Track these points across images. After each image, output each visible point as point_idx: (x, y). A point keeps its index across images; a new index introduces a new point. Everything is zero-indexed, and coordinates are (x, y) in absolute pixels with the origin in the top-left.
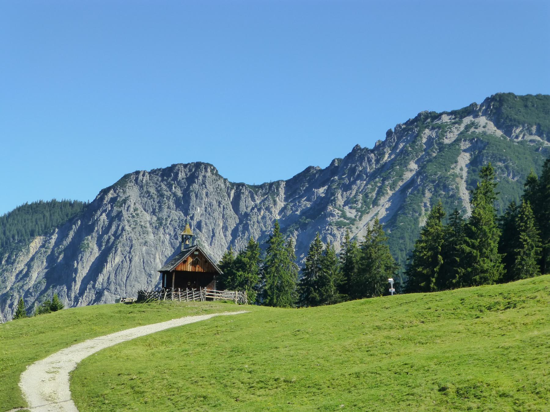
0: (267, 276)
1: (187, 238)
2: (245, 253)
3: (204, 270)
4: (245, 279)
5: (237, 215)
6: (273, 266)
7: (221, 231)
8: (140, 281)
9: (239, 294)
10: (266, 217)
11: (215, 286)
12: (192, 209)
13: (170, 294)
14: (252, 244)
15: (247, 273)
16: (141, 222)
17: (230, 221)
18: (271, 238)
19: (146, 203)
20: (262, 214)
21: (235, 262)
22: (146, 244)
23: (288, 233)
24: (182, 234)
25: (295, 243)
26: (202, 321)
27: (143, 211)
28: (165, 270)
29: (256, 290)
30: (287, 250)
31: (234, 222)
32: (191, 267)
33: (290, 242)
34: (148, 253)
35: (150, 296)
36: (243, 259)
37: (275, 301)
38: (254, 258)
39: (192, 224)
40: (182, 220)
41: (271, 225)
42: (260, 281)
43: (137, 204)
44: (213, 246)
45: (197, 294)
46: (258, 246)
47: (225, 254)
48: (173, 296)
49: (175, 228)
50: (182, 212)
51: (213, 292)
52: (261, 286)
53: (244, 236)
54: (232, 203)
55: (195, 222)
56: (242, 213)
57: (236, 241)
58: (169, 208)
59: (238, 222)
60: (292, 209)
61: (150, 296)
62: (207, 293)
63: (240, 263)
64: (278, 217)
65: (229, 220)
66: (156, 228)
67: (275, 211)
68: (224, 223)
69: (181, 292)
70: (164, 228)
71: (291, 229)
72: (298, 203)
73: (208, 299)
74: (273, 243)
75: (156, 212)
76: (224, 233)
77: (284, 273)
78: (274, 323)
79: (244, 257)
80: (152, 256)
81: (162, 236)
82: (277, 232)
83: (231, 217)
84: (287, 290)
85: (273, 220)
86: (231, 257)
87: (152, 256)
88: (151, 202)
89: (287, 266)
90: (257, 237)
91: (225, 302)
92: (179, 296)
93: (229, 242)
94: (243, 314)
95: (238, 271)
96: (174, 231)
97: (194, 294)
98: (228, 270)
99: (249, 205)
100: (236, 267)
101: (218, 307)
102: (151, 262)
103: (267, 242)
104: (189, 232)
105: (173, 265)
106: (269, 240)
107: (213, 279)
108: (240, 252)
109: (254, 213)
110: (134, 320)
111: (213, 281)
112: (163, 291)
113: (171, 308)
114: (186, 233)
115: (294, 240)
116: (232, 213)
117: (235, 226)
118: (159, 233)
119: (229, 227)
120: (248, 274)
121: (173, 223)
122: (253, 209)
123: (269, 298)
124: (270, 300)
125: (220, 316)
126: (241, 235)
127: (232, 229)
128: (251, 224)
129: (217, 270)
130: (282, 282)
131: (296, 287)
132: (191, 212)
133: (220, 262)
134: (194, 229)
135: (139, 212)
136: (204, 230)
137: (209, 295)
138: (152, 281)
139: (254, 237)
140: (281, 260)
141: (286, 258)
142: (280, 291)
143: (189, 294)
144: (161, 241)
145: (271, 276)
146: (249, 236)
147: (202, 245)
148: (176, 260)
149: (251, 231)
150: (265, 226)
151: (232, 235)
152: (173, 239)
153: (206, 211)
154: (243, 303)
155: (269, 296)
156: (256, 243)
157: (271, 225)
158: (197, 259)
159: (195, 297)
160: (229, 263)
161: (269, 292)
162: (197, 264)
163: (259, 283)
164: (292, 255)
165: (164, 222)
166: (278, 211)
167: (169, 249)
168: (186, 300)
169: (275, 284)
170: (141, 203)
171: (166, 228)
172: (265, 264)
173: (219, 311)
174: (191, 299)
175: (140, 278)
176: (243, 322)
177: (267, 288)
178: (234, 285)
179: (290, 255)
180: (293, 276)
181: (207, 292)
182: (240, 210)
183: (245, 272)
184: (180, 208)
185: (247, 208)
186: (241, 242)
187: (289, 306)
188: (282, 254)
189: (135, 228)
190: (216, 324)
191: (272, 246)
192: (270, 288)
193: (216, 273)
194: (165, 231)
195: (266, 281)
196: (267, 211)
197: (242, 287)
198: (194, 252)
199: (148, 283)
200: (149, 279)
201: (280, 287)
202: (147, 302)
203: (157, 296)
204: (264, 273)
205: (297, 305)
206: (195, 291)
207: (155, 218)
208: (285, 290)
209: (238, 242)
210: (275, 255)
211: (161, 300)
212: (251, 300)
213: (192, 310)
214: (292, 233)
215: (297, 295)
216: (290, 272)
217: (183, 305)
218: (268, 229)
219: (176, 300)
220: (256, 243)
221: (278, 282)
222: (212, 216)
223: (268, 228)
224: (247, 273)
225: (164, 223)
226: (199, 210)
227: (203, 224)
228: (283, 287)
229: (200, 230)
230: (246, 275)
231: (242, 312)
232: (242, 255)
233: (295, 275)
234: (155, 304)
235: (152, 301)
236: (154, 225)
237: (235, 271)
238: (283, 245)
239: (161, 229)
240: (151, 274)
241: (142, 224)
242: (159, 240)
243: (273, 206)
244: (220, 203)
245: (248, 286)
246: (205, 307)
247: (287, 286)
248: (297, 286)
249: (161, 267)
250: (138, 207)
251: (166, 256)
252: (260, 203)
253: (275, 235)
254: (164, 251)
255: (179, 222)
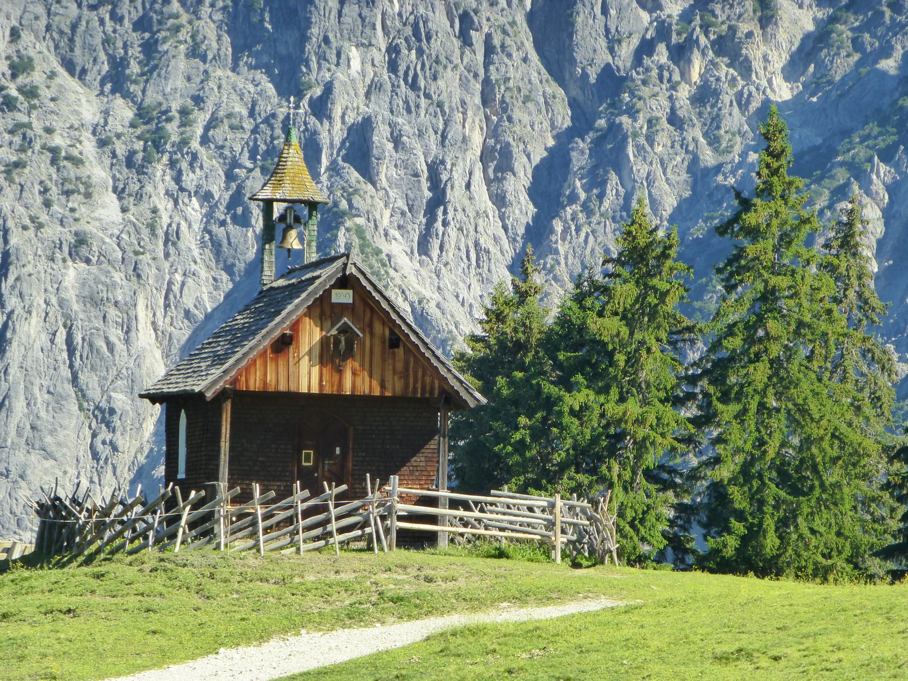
0: (727, 411)
1: (290, 219)
2: (605, 290)
3: (383, 386)
4: (608, 426)
5: (562, 83)
6: (758, 357)
7: (478, 175)
8: (53, 448)
9: (571, 508)
10: (716, 93)
11: (445, 469)
12: (322, 57)
13: (209, 517)
14: (642, 242)
15: (614, 393)
16: (49, 131)
17: (526, 119)
18: (746, 205)
19: (74, 27)
20: (695, 76)
21: (550, 343)
22: (84, 251)
23: (841, 175)
24: (261, 196)
25: (877, 228)
26: (379, 655)
27: (61, 70)
28: (181, 387)
29: (666, 486)
30: (830, 268)
31: (546, 124)
32: (316, 370)
33: (850, 225)
34: (93, 300)
35: (100, 527)
36: (594, 324)
37: (771, 542)
38: (653, 315)
39: (324, 138)
40: (266, 121)
41: (743, 135)
42: (688, 440)
43: (27, 38)
44: (435, 253)
45: (349, 514)
46: (673, 253)
47: (495, 300)
48: (221, 528)
49: (235, 163)
50: (269, 73)
51: (432, 501)
52: (694, 462)
53: (601, 197)
54: (531, 18)
55: (338, 125)
56: (585, 75)
57: (558, 226)
58: (195, 52)
59: (568, 123)
60: (857, 44)
61: (100, 527)
62: (403, 508)
63: (576, 347)
64: (783, 92)
65: (517, 114)
66: (130, 162)
67: (766, 59)
68: (494, 132)
69: (265, 503)
70: (172, 163)
71: (860, 152)
72: (888, 13)
73: (409, 540)
74: (754, 233)
75: (128, 78)
76: (494, 183)
77: (816, 394)
78: (764, 662)
79: (600, 314)
80: (112, 312)
81: (164, 205)
82: (775, 172)
83: (527, 99)
84: (837, 485)
85: (755, 105)
86: (529, 316)
87: (112, 312)
88: (102, 22)
89: (834, 352)
90: (670, 203)
91: (501, 554)
92: (254, 524)
93: (521, 231)
94: (596, 614)
95: (570, 388)
96: (230, 177)
97: (334, 512)
98: (512, 383)
99: (624, 28)
100: (558, 365)
101: (462, 583)
102: (111, 347)
103: (722, 230)
104: (302, 184)
105: (219, 360)
106: (736, 218)
107: (431, 432)
108: (578, 286)
109: (655, 73)
110: (21, 658)
111: (432, 445)
112: (171, 503)
113: (212, 587)
114: (287, 191)
115: (872, 213)
116: (534, 76)
117: (551, 143)
118: (149, 188)
119: (517, 150)
120: (622, 399)
121: (217, 134)
122: (646, 48)
123: (739, 527)
124: (744, 539)
125: (474, 632)
126: (583, 196)
127: (536, 159)
128: (635, 135)
129: (453, 382)
130: (807, 442)
131: (883, 465)
132: (313, 76)
133: (475, 339)
134: (334, 168)
135: (37, 77)
136: (386, 172)
137: (412, 517)
138: (120, 442)
139: (655, 204)
140: (801, 324)
141: (829, 312)
142: (795, 491)
143: (306, 514)
144: (161, 233)
145: (745, 411)
146: (628, 198)
147: (378, 252)
148: (238, 336)
149: (640, 169)
150: (713, 141)
151: (534, 193)
152: (223, 223)
153: (393, 67)
154: (597, 558)
155: (740, 516)
156: (661, 234)
157: (743, 135)
158: (345, 330)
159: (341, 531)
160: (520, 346)
161: (738, 498)
162: (349, 353)
163: (681, 447)
164: (860, 295)
165: (172, 128)
166: (785, 57)
167: (203, 273)
168: (292, 543)
169: (771, 454)
170: (48, 28)
171: (184, 165)
172: (716, 346)
173: (474, 602)
174: (317, 538)
175: (52, 432)
176: (594, 656)
177: (724, 473)
178: (546, 459)
179: (851, 294)
180: (868, 410)
181: (403, 498)
182: (578, 57)
183: (605, 390)
184: (257, 55)
185: (613, 43)
186: (585, 229)
187: (849, 568)
188: (805, 289)
189: (18, 165)
190: (452, 668)
191: (751, 250)
192: (746, 473)
193: (451, 400)
194: (178, 179)
195: (719, 440)
196: (723, 61)
197: (593, 471)
198: (328, 293)
199: (95, 456)
200: (105, 435)
201: (798, 469)
202: (89, 561)
203: (140, 526)
204: (706, 395)
205: (891, 565)
206: (341, 498)
207: (124, 111)
208: (822, 485)
209: (566, 230)
210: (768, 296)
211: (163, 549)
212: (643, 539)
213: (326, 597)
214: (859, 173)
215: (893, 510)
216: (850, 386)
217: (278, 574)
218: (728, 158)
219: (239, 544)
220: (661, 234)
221: (783, 445)
222: (428, 96)
223: (728, 150)
224: (614, 393)
225: (175, 138)
226: (356, 65)
227: (381, 136)
228: (815, 469)
229: (368, 173)
230: (613, 409)
231: (592, 606)
232: (588, 302)
233: (876, 400)
234: (131, 573)
235: (113, 552)
236: (121, 149)
237: (554, 390)
238: (809, 242)
239: (160, 170)
240: (112, 411)
241: (58, 140)
242: (152, 228)
243: (757, 31)
244: (466, 23)
245: (623, 466)
246: (397, 583)
247: (835, 460)
248: (891, 460)
249: (161, 371)
250: (31, 53)
251: (187, 314)
252: (686, 17)
253: (766, 192)
254: (176, 288)
255: (255, 131)
